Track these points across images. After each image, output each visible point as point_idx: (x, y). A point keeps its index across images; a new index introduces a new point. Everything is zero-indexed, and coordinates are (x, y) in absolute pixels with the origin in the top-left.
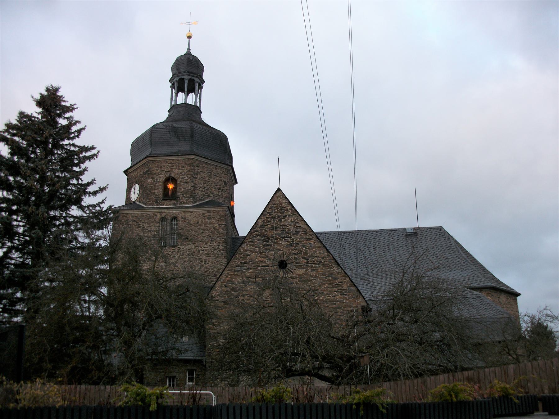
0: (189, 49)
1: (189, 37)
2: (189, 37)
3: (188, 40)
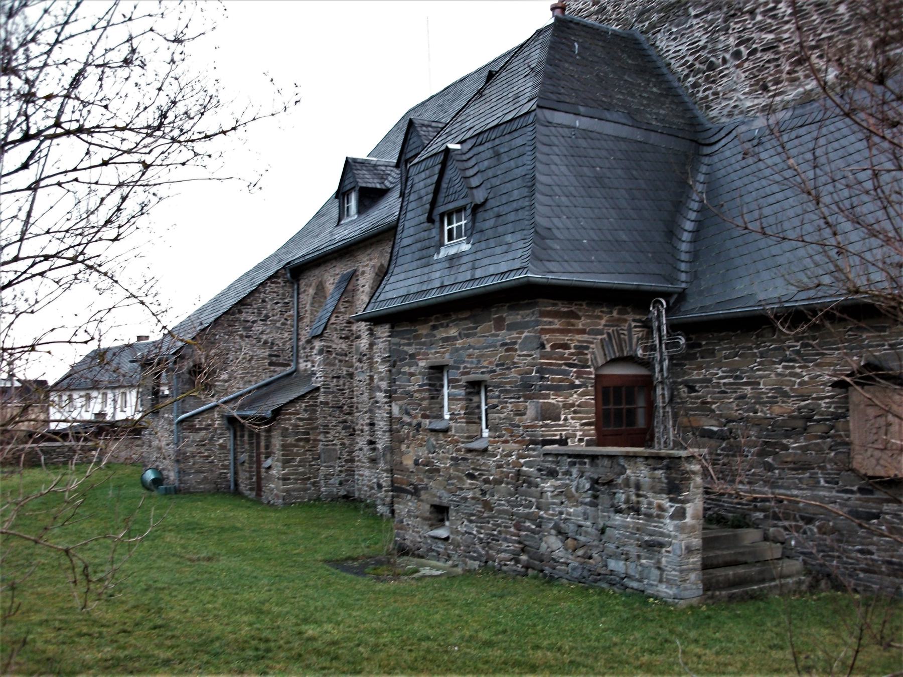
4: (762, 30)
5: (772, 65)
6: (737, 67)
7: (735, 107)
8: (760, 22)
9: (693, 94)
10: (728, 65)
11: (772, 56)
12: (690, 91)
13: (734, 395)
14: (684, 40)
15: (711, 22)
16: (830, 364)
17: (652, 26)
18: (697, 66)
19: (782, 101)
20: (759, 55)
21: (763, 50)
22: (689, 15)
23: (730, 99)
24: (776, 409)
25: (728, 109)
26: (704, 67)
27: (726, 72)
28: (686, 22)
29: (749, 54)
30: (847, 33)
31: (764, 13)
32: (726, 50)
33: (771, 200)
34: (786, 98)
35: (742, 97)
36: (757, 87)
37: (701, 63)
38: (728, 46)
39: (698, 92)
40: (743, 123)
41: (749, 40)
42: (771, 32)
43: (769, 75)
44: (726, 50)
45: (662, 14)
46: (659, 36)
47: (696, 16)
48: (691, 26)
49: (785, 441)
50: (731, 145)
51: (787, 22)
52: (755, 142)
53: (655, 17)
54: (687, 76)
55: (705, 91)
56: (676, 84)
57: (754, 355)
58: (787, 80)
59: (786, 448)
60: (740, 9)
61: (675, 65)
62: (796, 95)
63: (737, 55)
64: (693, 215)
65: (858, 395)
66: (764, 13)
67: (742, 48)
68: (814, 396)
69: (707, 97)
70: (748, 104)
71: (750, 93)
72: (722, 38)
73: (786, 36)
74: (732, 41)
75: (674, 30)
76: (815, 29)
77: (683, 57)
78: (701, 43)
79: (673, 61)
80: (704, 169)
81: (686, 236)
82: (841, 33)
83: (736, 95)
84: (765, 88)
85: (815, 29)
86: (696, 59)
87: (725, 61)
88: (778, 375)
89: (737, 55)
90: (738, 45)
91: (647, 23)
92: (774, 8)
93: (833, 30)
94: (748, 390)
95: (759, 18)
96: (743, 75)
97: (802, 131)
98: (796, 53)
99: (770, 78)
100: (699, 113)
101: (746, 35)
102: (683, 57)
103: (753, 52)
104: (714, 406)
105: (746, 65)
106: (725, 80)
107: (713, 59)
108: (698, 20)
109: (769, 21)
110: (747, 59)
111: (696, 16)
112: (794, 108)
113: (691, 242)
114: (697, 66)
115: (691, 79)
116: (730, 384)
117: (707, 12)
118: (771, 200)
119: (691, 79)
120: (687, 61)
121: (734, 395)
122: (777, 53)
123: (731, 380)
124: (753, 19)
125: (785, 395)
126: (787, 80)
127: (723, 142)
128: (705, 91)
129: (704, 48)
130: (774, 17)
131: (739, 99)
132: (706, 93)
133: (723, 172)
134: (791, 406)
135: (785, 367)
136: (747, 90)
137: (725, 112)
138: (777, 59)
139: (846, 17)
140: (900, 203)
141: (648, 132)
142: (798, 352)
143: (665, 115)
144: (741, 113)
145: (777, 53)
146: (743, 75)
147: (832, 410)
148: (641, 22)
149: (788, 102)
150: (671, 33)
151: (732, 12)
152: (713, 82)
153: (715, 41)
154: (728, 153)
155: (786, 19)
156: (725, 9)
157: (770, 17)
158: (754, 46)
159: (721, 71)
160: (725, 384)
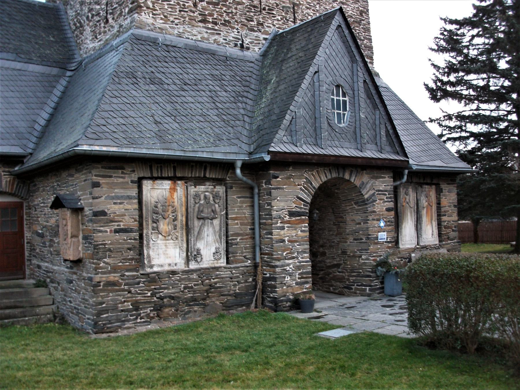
89: (88, 18)
141: (27, 64)
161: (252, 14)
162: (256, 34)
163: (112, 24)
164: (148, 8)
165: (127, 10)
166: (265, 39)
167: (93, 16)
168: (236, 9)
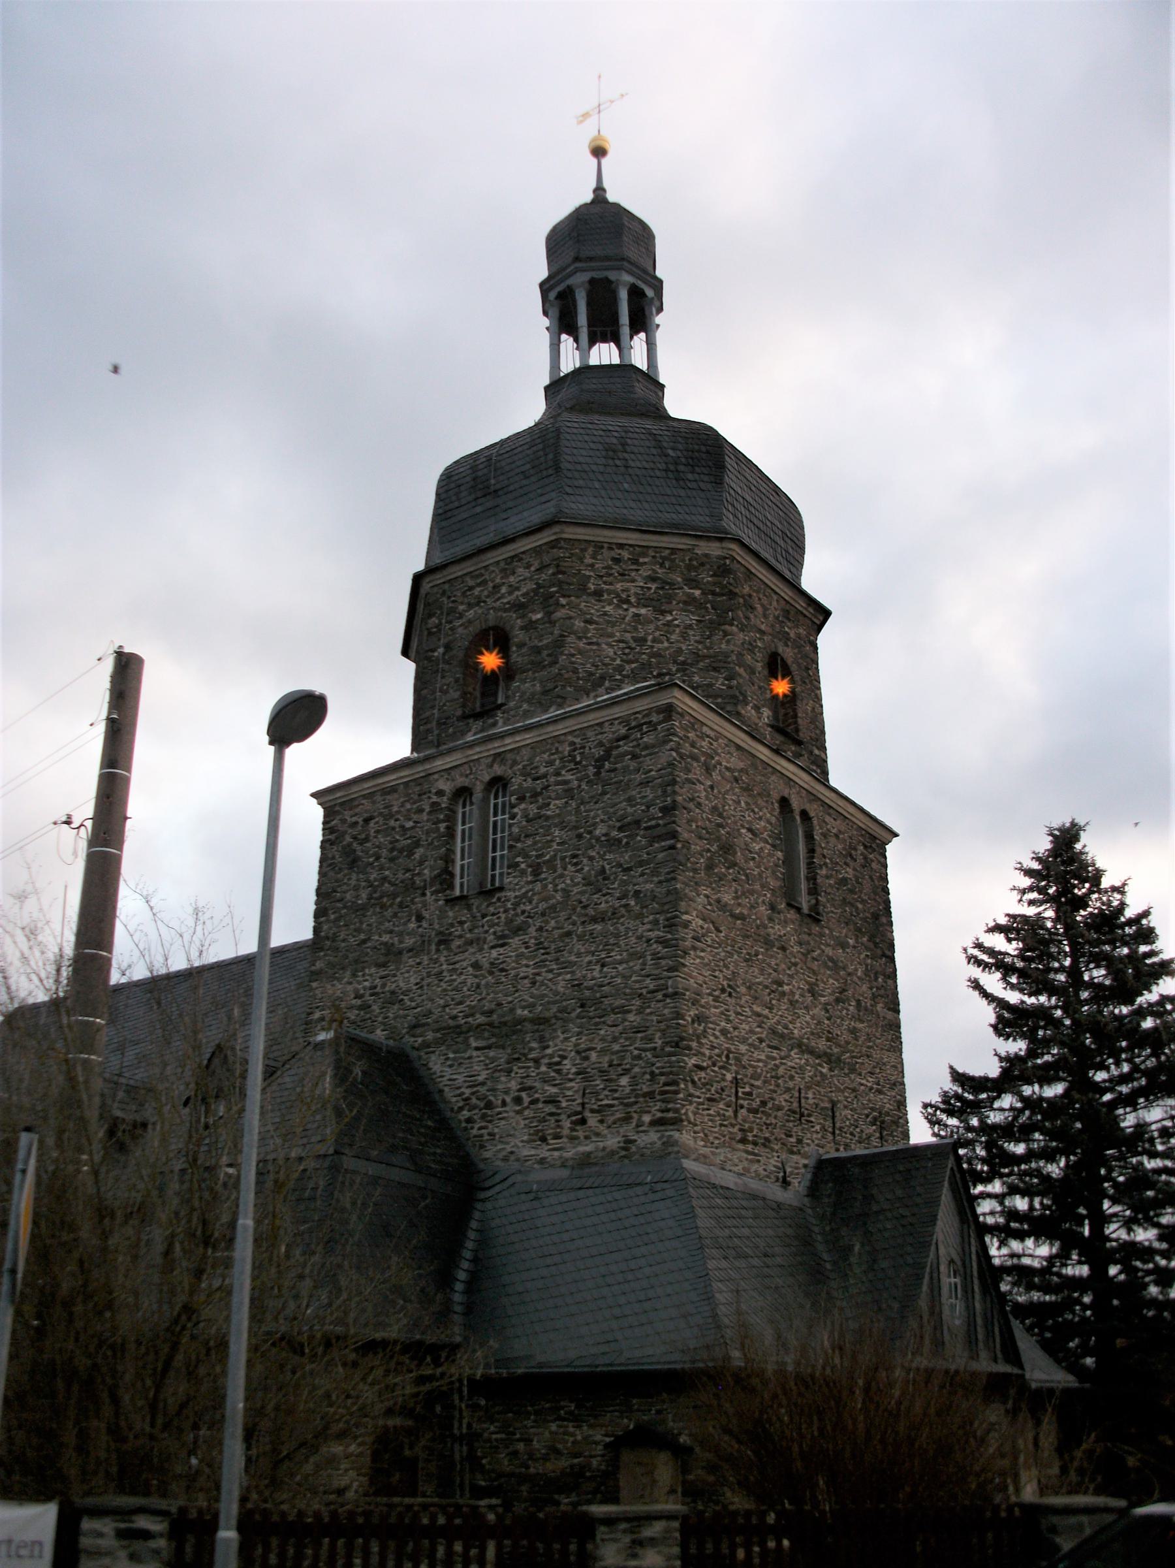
0: (599, 190)
1: (599, 152)
2: (599, 152)
3: (594, 161)
4: (545, 1082)
5: (552, 1119)
6: (518, 1112)
7: (512, 1153)
8: (544, 1073)
9: (466, 1129)
10: (507, 1109)
11: (554, 1110)
12: (464, 1125)
13: (507, 1451)
14: (462, 1070)
15: (493, 1060)
16: (602, 1426)
17: (426, 1045)
18: (474, 1101)
19: (561, 1157)
20: (540, 1105)
21: (545, 1102)
22: (468, 1045)
23: (508, 1143)
24: (549, 1465)
25: (504, 1153)
26: (482, 1104)
27: (505, 1115)
28: (465, 1051)
29: (532, 1102)
30: (627, 1105)
31: (550, 1065)
32: (507, 1092)
33: (549, 1261)
34: (565, 1155)
35: (520, 1144)
36: (535, 1137)
37: (478, 1099)
38: (509, 1089)
39: (472, 1128)
40: (520, 1172)
41: (531, 1088)
42: (555, 1085)
43: (549, 1128)
44: (507, 1092)
45: (439, 1035)
46: (433, 1057)
47: (477, 1049)
48: (470, 1058)
49: (556, 1497)
50: (506, 1193)
51: (571, 1080)
52: (532, 1196)
53: (430, 1036)
54: (461, 1109)
55: (480, 1129)
56: (448, 1114)
57: (529, 1413)
58: (567, 1137)
59: (558, 1503)
60: (525, 1055)
61: (449, 1094)
62: (576, 1154)
63: (518, 1100)
64: (465, 1265)
65: (627, 1457)
66: (550, 1065)
67: (524, 1095)
68: (587, 1454)
69: (481, 1136)
70: (526, 1152)
71: (528, 1142)
72: (503, 1079)
73: (569, 1093)
74: (514, 1085)
75: (451, 1055)
76: (597, 1093)
77: (459, 1088)
78: (481, 1078)
79: (446, 1089)
80: (477, 1215)
81: (459, 1287)
82: (622, 1103)
83: (513, 1141)
84: (544, 1139)
85: (597, 1093)
86: (473, 1093)
87: (504, 1103)
88: (551, 1433)
90: (519, 1090)
91: (420, 1040)
92: (558, 1063)
93: (614, 1099)
94: (521, 1446)
95: (543, 1069)
96: (523, 1123)
97: (581, 1194)
98: (577, 1113)
99: (551, 1131)
100: (473, 1151)
101: (529, 1083)
102: (459, 1088)
103: (534, 1102)
104: (484, 1461)
105: (526, 1113)
106: (503, 1122)
107: (492, 1098)
108: (479, 1053)
109: (553, 1074)
110: (528, 1107)
111: (477, 1049)
112: (573, 1168)
113: (463, 1293)
114: (474, 1101)
115: (466, 1113)
116: (502, 1439)
117: (489, 1047)
118: (549, 1261)
119: (466, 1113)
120: (463, 1093)
121: (507, 1451)
122: (559, 1108)
123: (503, 1436)
124: (538, 1068)
125: (558, 1452)
126: (567, 1137)
127: (497, 1189)
128: (480, 1129)
129: (483, 1084)
130: (558, 1072)
131: (516, 1146)
132: (483, 1131)
133: (497, 1221)
134: (564, 1463)
135: (559, 1426)
136: (525, 1138)
137: (501, 1156)
138: (559, 1114)
139: (628, 1090)
140: (482, 1561)
142: (571, 1413)
143: (441, 1155)
144: (518, 1160)
145: (559, 1108)
146: (523, 1123)
147: (603, 1467)
148: (414, 1036)
149: (567, 1160)
150: (447, 1059)
151: (516, 1056)
152: (490, 1122)
153: (496, 1080)
154: (502, 1202)
155: (570, 1076)
156: (509, 1051)
157: (555, 1071)
158: (536, 1096)
159: (500, 1113)
160: (496, 1440)
161: (791, 1124)
162: (795, 1157)
163: (597, 1130)
164: (690, 1122)
165: (647, 1118)
166: (805, 1166)
167: (534, 1102)
168: (776, 1117)
